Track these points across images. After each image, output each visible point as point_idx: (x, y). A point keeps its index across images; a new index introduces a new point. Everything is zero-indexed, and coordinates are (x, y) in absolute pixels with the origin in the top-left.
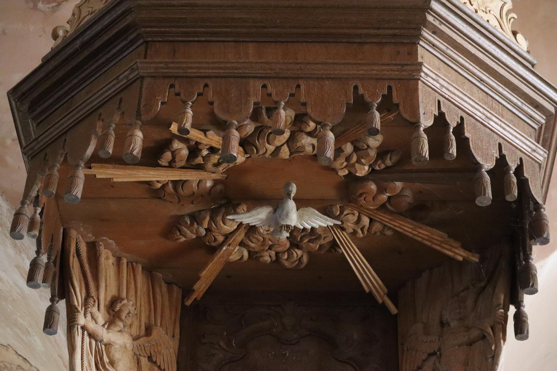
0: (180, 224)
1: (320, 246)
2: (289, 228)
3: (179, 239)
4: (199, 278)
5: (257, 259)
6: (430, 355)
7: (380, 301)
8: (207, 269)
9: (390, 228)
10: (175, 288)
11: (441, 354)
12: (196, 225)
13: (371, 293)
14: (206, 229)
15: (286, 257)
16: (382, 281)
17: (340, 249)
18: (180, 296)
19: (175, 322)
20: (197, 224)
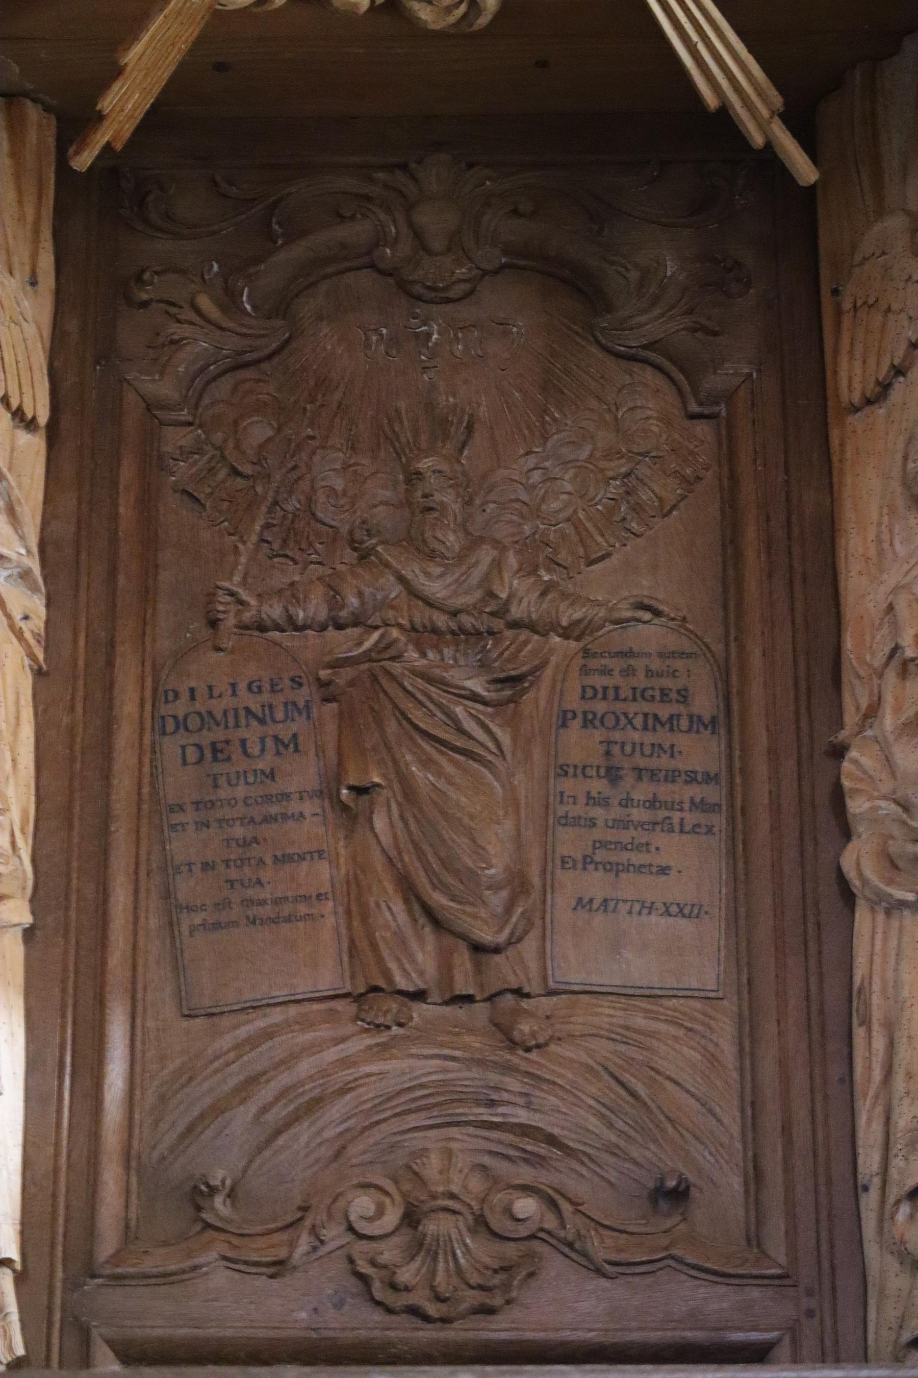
4: (118, 72)
7: (758, 140)
10: (33, 112)
13: (724, 110)
18: (51, 142)
19: (36, 232)
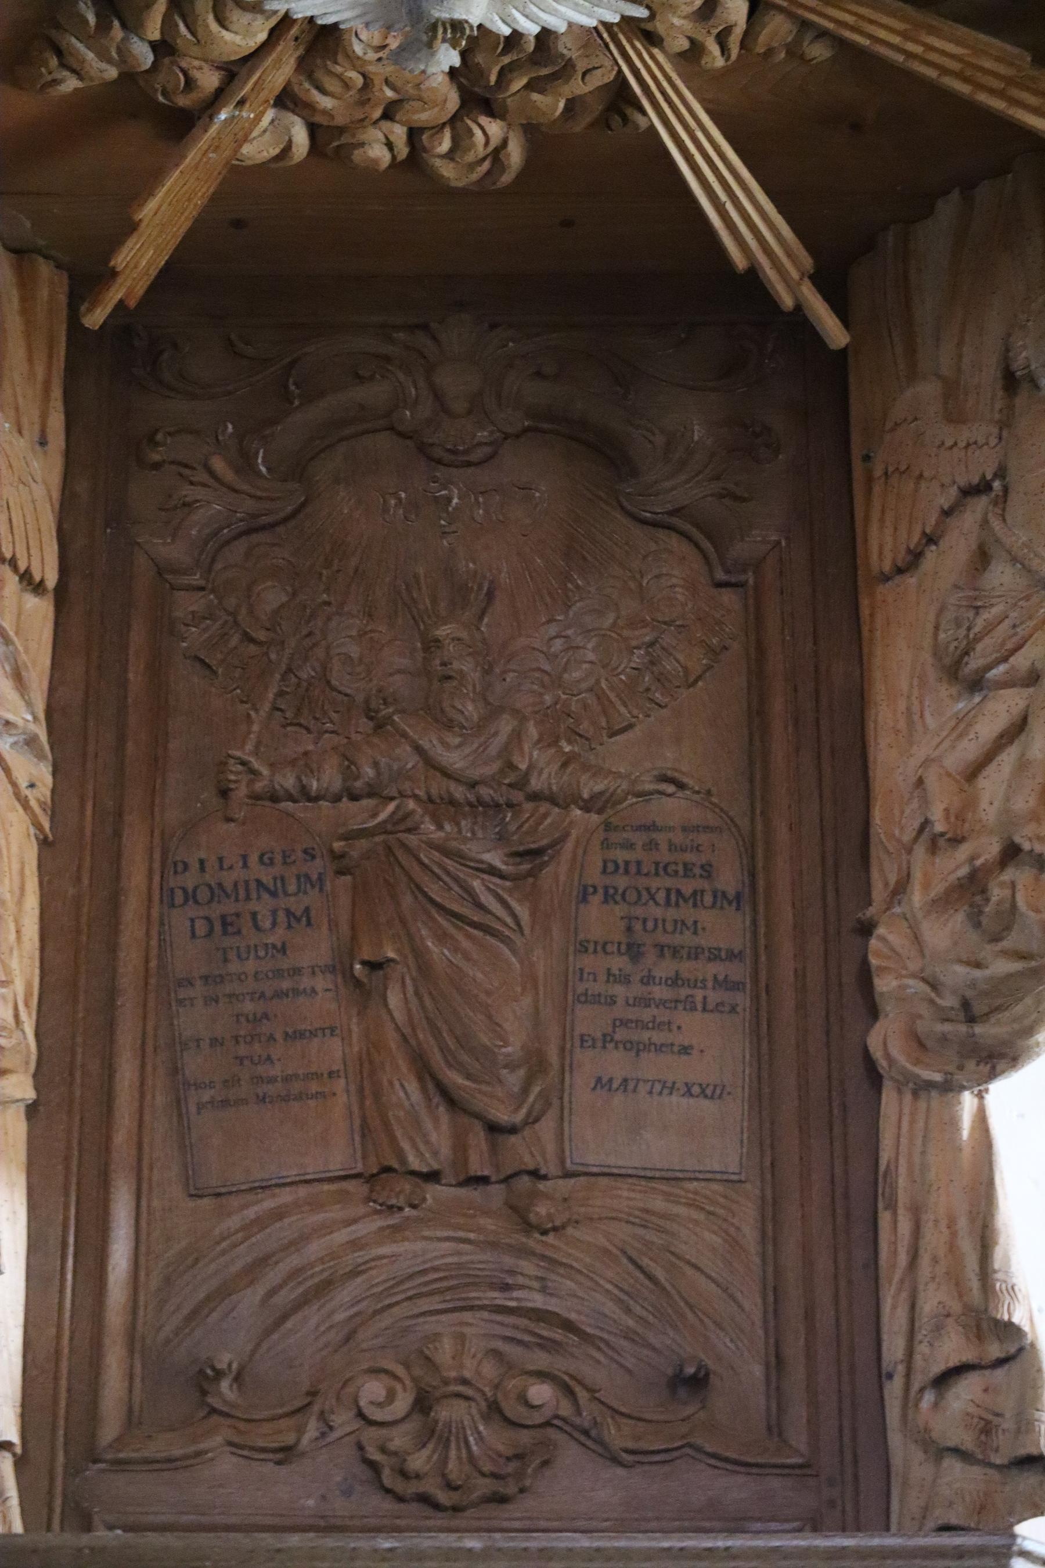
0: (58, 26)
1: (571, 104)
2: (463, 31)
3: (55, 82)
4: (132, 227)
5: (343, 154)
6: (970, 492)
7: (788, 302)
8: (161, 193)
9: (823, 34)
10: (45, 269)
11: (1006, 490)
12: (117, 32)
13: (753, 272)
14: (154, 46)
15: (446, 145)
16: (795, 230)
17: (644, 113)
18: (63, 299)
20: (124, 26)
